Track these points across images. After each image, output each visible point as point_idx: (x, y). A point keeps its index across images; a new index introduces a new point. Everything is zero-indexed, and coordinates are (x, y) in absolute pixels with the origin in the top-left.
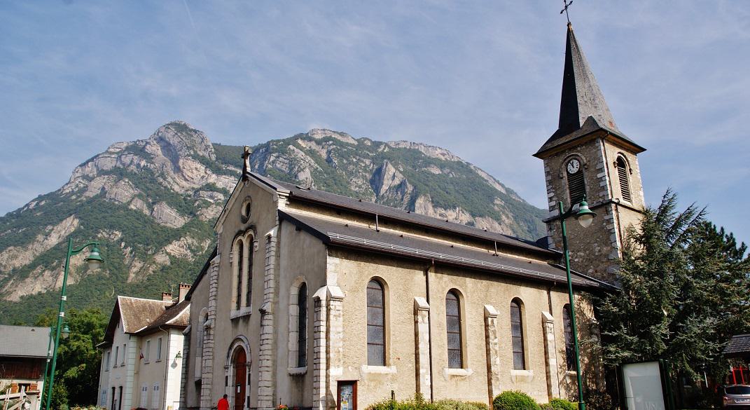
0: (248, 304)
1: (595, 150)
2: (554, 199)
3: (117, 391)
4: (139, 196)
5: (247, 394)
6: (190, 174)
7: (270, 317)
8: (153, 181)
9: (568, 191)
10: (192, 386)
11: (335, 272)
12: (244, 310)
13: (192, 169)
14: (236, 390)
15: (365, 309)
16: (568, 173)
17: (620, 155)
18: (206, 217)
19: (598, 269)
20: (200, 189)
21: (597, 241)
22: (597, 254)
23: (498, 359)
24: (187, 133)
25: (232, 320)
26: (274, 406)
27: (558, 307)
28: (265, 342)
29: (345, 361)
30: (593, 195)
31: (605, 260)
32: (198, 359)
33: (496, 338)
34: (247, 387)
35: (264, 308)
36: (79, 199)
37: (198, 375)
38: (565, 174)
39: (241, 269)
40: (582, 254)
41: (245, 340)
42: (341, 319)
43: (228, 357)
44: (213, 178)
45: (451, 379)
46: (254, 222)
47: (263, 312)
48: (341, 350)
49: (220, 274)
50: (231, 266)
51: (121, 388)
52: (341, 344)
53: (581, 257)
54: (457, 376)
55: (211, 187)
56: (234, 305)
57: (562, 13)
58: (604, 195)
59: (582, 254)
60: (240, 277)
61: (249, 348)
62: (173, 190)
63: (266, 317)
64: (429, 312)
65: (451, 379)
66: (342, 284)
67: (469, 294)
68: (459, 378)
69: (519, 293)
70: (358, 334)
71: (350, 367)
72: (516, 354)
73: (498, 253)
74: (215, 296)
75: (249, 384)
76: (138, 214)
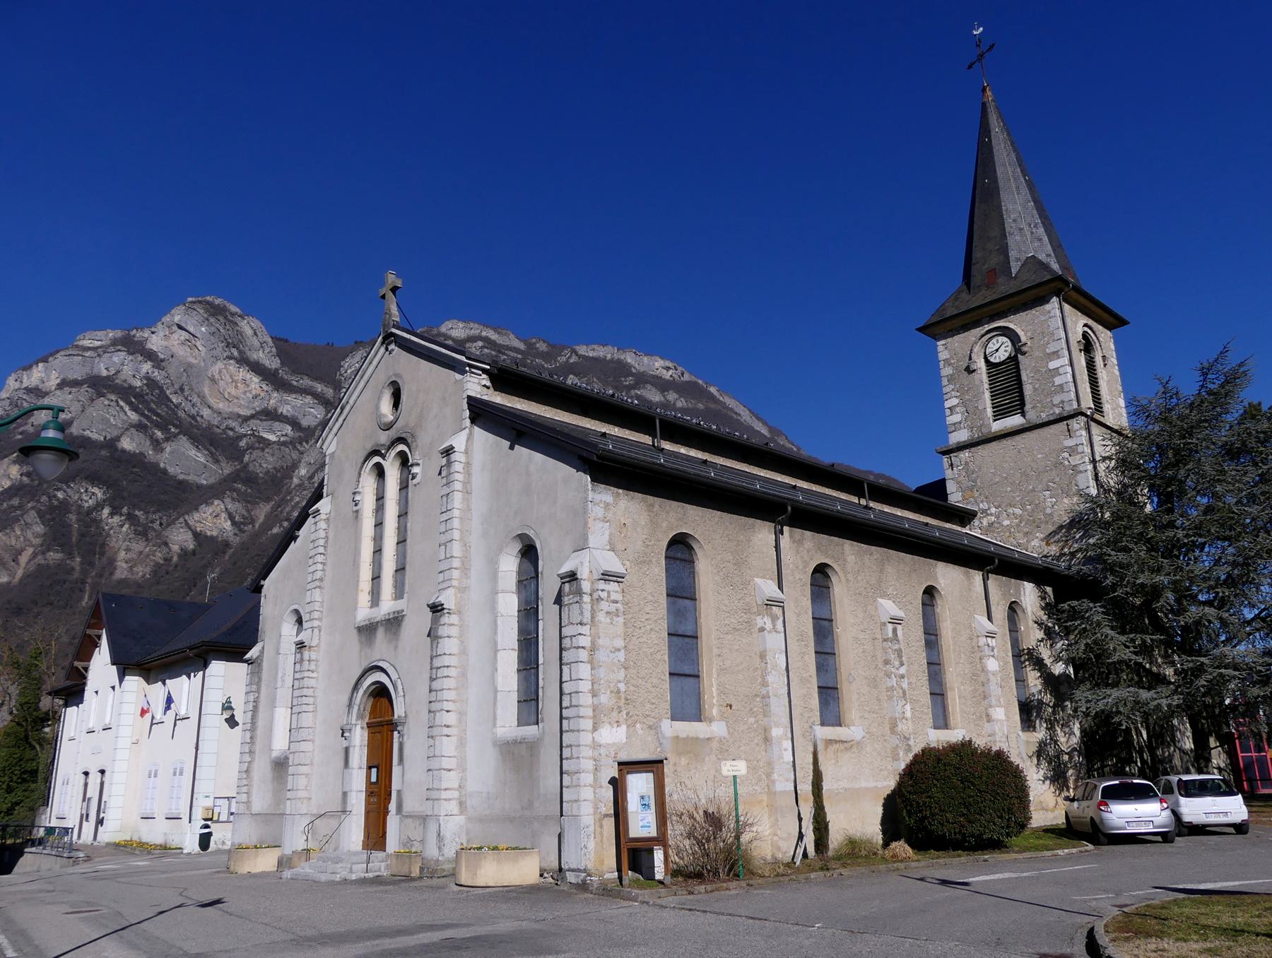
0: (399, 593)
1: (1043, 318)
2: (958, 409)
3: (94, 779)
4: (140, 427)
5: (395, 786)
6: (233, 392)
7: (454, 619)
8: (164, 399)
9: (987, 395)
10: (262, 769)
11: (605, 520)
12: (388, 605)
13: (236, 382)
14: (369, 776)
15: (663, 600)
17: (1086, 329)
18: (260, 465)
20: (252, 417)
21: (1048, 486)
23: (908, 707)
24: (226, 318)
26: (461, 813)
27: (1000, 608)
28: (445, 672)
29: (625, 708)
30: (1039, 402)
32: (584, 671)
33: (902, 664)
34: (396, 771)
35: (442, 599)
36: (21, 429)
37: (280, 743)
38: (981, 364)
39: (379, 525)
41: (390, 670)
42: (621, 620)
43: (350, 705)
44: (275, 399)
47: (436, 609)
48: (622, 687)
49: (331, 535)
50: (357, 517)
51: (150, 777)
52: (622, 674)
54: (836, 742)
55: (270, 415)
56: (364, 598)
57: (970, 67)
58: (1063, 402)
59: (1018, 511)
60: (378, 539)
61: (400, 688)
62: (202, 417)
63: (445, 619)
64: (783, 607)
66: (620, 547)
67: (850, 577)
68: (842, 746)
69: (936, 579)
70: (651, 654)
71: (638, 725)
73: (872, 504)
74: (321, 580)
76: (135, 461)
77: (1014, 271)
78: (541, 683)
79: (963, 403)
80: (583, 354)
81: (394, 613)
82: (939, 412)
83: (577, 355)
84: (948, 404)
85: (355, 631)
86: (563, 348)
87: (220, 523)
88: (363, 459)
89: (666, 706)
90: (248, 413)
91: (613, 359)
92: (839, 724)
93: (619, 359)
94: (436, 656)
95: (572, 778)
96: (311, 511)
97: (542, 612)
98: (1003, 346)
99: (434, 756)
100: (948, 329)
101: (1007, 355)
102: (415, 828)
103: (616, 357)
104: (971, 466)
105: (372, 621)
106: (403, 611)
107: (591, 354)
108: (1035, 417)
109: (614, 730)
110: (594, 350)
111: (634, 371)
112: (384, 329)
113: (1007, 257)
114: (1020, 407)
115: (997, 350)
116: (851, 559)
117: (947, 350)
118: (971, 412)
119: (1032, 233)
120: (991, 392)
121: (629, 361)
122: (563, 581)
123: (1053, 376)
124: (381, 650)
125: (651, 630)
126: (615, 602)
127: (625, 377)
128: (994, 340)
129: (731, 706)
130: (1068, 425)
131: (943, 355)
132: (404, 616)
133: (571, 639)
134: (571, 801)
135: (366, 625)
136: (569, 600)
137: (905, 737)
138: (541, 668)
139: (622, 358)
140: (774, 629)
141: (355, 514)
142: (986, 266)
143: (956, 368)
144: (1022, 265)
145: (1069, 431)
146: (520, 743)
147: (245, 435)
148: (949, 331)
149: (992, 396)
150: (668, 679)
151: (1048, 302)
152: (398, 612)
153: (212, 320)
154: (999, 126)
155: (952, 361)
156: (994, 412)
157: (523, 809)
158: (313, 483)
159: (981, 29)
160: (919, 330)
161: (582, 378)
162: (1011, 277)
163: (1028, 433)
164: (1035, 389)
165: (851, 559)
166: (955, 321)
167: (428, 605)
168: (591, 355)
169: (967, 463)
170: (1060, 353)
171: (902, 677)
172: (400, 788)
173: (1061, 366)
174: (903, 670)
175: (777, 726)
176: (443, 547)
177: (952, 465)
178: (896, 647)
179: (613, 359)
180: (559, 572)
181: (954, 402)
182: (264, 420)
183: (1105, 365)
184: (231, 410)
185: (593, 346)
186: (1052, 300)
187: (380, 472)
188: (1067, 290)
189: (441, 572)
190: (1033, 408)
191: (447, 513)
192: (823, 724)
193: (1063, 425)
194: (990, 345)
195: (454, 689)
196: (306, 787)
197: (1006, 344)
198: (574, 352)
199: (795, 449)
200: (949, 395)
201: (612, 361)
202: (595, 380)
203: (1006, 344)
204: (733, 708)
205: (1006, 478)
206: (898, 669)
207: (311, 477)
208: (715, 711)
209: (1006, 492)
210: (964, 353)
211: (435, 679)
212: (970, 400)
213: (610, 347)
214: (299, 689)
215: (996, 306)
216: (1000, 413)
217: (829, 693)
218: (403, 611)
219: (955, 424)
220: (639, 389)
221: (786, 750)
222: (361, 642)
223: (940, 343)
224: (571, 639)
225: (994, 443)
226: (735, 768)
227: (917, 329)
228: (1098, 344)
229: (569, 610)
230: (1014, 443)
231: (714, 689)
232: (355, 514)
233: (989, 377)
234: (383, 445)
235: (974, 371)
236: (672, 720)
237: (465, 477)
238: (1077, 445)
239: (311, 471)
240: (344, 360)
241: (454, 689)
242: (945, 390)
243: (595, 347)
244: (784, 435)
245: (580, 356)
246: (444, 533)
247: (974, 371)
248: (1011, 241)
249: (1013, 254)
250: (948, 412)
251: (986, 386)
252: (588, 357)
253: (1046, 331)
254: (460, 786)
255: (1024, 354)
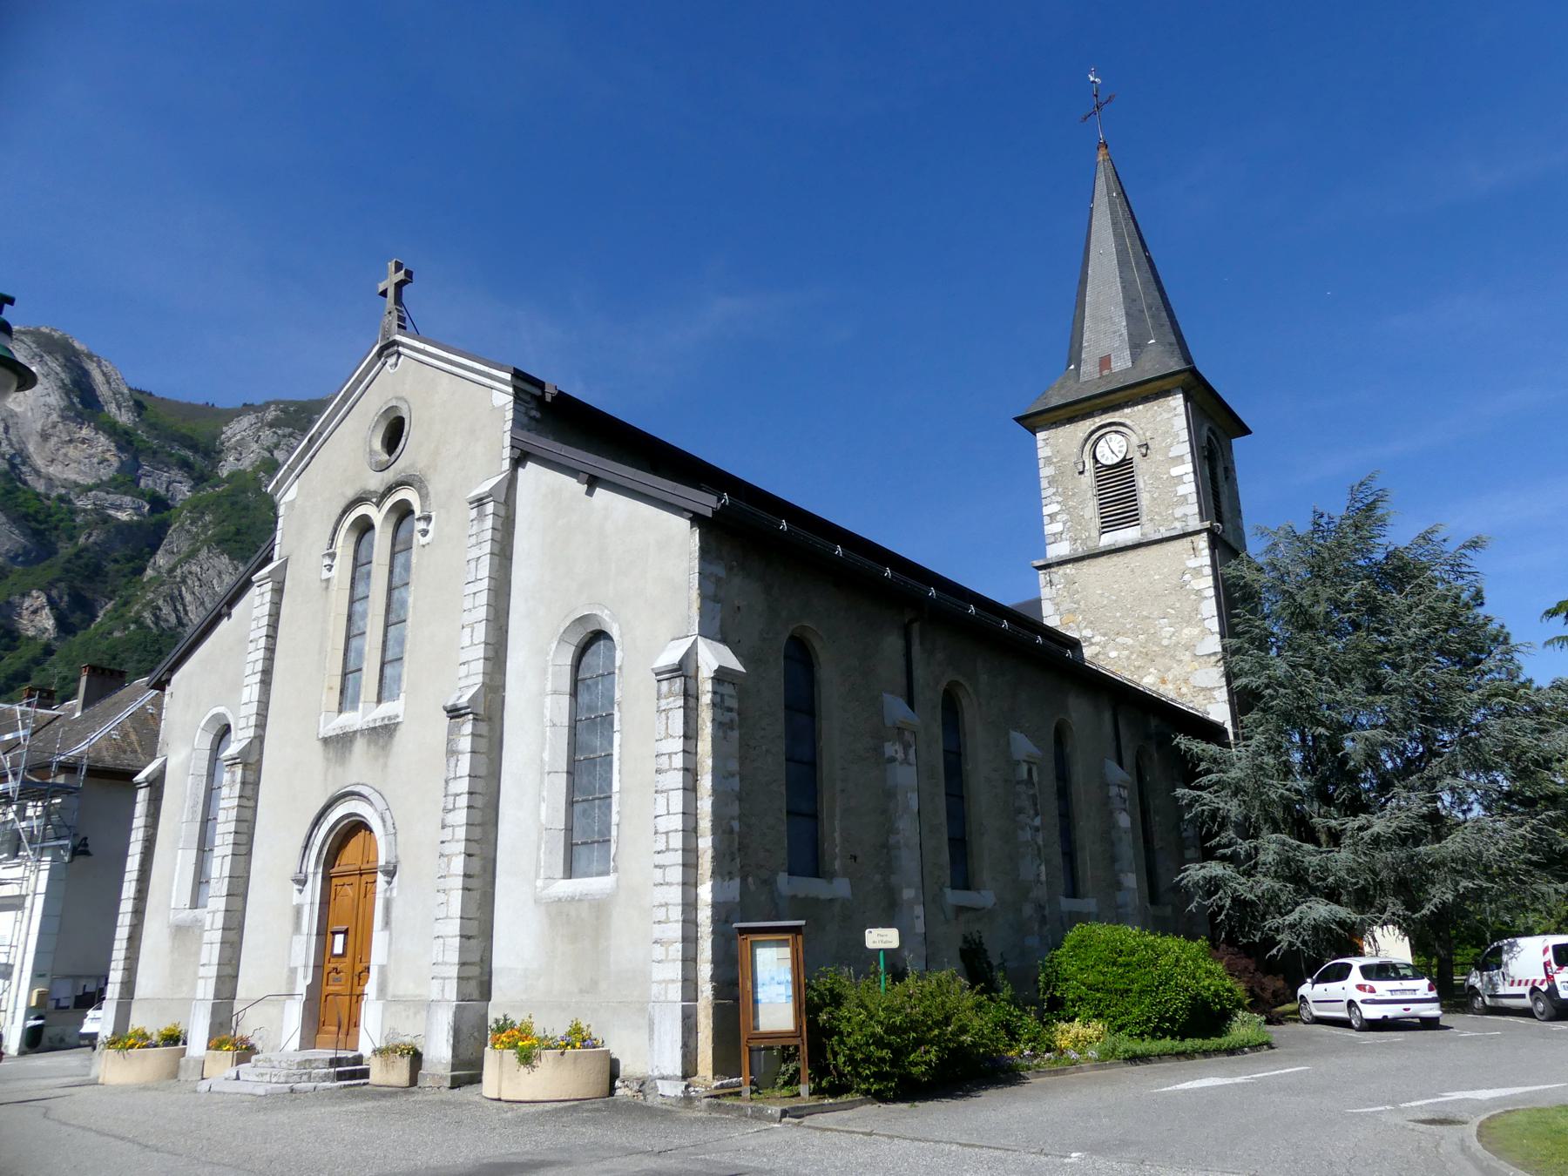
16: (1097, 461)
19: (1170, 676)
20: (97, 486)
22: (1165, 642)
23: (1043, 868)
25: (326, 741)
30: (1159, 514)
31: (1187, 657)
33: (1037, 814)
40: (1130, 641)
41: (374, 797)
45: (957, 917)
46: (420, 465)
50: (327, 588)
53: (1125, 647)
59: (1130, 641)
65: (957, 917)
72: (580, 864)
75: (387, 923)
78: (615, 818)
79: (1066, 509)
81: (383, 719)
82: (1035, 521)
84: (1046, 511)
85: (318, 746)
87: (40, 621)
88: (340, 511)
89: (782, 855)
90: (90, 481)
92: (967, 887)
94: (455, 778)
95: (667, 950)
96: (254, 578)
97: (620, 720)
99: (447, 918)
102: (408, 1017)
105: (348, 729)
106: (397, 716)
109: (726, 883)
112: (384, 335)
114: (1129, 516)
116: (984, 678)
117: (1048, 443)
118: (1075, 521)
122: (658, 677)
123: (1177, 485)
124: (359, 768)
125: (767, 751)
126: (730, 710)
129: (855, 858)
131: (1043, 452)
132: (398, 723)
133: (670, 757)
134: (664, 981)
135: (338, 735)
136: (668, 704)
137: (1040, 906)
138: (615, 799)
140: (906, 761)
141: (324, 585)
146: (580, 900)
147: (85, 511)
150: (785, 818)
152: (390, 718)
153: (47, 358)
155: (1055, 460)
157: (581, 991)
158: (175, 577)
160: (1018, 420)
165: (984, 678)
167: (445, 708)
171: (1037, 829)
172: (385, 963)
174: (1037, 822)
175: (909, 886)
176: (468, 630)
178: (1031, 792)
180: (654, 666)
181: (1054, 508)
182: (113, 493)
184: (65, 476)
187: (364, 527)
189: (464, 664)
190: (1152, 520)
191: (476, 583)
192: (954, 887)
195: (479, 825)
196: (230, 961)
200: (1048, 500)
204: (858, 860)
205: (1116, 601)
206: (1033, 820)
207: (171, 571)
208: (837, 865)
209: (1115, 617)
211: (450, 811)
212: (1075, 508)
214: (225, 823)
215: (1112, 397)
216: (1108, 525)
217: (960, 845)
218: (397, 716)
219: (1054, 534)
221: (918, 917)
222: (328, 760)
223: (1041, 436)
224: (670, 757)
226: (885, 939)
227: (1015, 419)
229: (668, 718)
231: (837, 835)
232: (324, 585)
234: (376, 492)
236: (789, 874)
237: (503, 537)
238: (1201, 566)
239: (172, 562)
240: (226, 425)
241: (479, 825)
242: (1044, 494)
246: (470, 610)
250: (1046, 520)
254: (482, 960)
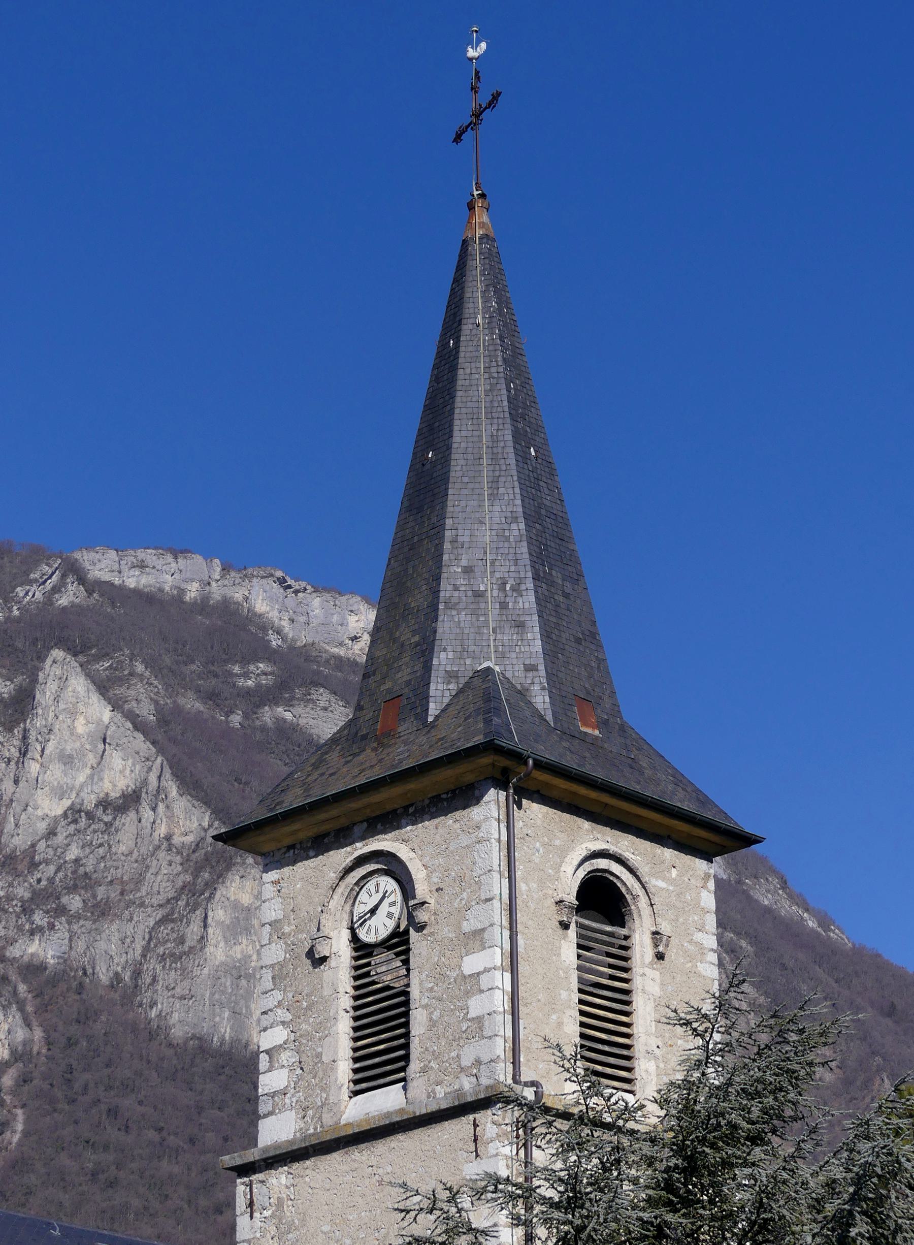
1: (465, 840)
9: (344, 1026)
77: (434, 709)
80: (106, 577)
83: (82, 579)
86: (37, 555)
91: (205, 599)
93: (226, 602)
98: (386, 902)
100: (288, 841)
101: (391, 925)
103: (217, 592)
104: (289, 1211)
107: (132, 580)
108: (424, 1096)
110: (142, 566)
111: (275, 641)
113: (427, 668)
115: (373, 911)
119: (503, 606)
120: (356, 1019)
121: (261, 606)
123: (468, 994)
127: (245, 661)
128: (371, 885)
130: (476, 1125)
139: (238, 596)
142: (388, 685)
143: (291, 948)
144: (460, 692)
145: (475, 1141)
148: (292, 847)
149: (355, 1029)
151: (477, 800)
154: (486, 309)
155: (287, 929)
156: (355, 1071)
159: (483, 45)
161: (98, 658)
162: (425, 723)
163: (400, 1137)
164: (432, 1024)
166: (296, 826)
168: (131, 583)
169: (280, 1204)
170: (486, 935)
173: (487, 970)
177: (251, 1204)
179: (205, 599)
183: (660, 956)
185: (141, 554)
186: (486, 798)
188: (522, 771)
193: (461, 1127)
194: (363, 896)
197: (392, 899)
198: (74, 570)
199: (811, 923)
200: (270, 1017)
201: (203, 606)
202: (140, 668)
203: (392, 899)
210: (311, 909)
212: (309, 1036)
213: (198, 559)
220: (289, 704)
225: (336, 1156)
228: (643, 902)
230: (373, 1161)
233: (356, 978)
235: (324, 959)
243: (148, 555)
244: (775, 872)
245: (91, 586)
247: (324, 959)
248: (445, 626)
249: (443, 660)
251: (347, 1002)
252: (122, 588)
253: (468, 873)
255: (420, 928)
